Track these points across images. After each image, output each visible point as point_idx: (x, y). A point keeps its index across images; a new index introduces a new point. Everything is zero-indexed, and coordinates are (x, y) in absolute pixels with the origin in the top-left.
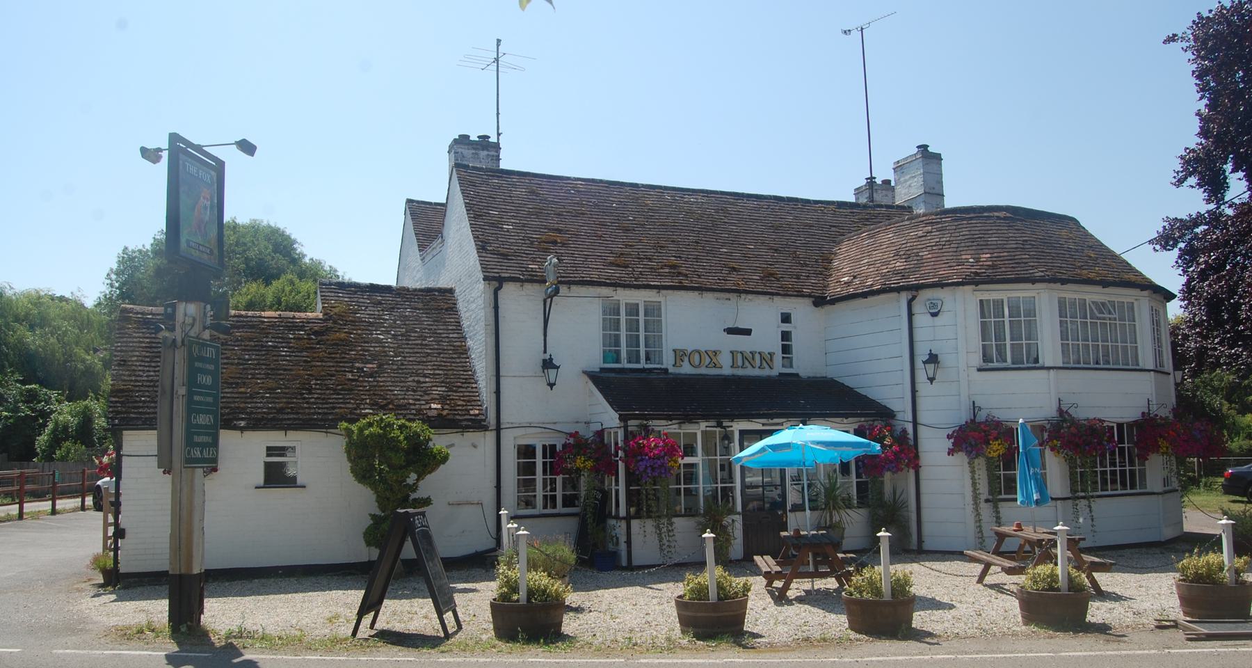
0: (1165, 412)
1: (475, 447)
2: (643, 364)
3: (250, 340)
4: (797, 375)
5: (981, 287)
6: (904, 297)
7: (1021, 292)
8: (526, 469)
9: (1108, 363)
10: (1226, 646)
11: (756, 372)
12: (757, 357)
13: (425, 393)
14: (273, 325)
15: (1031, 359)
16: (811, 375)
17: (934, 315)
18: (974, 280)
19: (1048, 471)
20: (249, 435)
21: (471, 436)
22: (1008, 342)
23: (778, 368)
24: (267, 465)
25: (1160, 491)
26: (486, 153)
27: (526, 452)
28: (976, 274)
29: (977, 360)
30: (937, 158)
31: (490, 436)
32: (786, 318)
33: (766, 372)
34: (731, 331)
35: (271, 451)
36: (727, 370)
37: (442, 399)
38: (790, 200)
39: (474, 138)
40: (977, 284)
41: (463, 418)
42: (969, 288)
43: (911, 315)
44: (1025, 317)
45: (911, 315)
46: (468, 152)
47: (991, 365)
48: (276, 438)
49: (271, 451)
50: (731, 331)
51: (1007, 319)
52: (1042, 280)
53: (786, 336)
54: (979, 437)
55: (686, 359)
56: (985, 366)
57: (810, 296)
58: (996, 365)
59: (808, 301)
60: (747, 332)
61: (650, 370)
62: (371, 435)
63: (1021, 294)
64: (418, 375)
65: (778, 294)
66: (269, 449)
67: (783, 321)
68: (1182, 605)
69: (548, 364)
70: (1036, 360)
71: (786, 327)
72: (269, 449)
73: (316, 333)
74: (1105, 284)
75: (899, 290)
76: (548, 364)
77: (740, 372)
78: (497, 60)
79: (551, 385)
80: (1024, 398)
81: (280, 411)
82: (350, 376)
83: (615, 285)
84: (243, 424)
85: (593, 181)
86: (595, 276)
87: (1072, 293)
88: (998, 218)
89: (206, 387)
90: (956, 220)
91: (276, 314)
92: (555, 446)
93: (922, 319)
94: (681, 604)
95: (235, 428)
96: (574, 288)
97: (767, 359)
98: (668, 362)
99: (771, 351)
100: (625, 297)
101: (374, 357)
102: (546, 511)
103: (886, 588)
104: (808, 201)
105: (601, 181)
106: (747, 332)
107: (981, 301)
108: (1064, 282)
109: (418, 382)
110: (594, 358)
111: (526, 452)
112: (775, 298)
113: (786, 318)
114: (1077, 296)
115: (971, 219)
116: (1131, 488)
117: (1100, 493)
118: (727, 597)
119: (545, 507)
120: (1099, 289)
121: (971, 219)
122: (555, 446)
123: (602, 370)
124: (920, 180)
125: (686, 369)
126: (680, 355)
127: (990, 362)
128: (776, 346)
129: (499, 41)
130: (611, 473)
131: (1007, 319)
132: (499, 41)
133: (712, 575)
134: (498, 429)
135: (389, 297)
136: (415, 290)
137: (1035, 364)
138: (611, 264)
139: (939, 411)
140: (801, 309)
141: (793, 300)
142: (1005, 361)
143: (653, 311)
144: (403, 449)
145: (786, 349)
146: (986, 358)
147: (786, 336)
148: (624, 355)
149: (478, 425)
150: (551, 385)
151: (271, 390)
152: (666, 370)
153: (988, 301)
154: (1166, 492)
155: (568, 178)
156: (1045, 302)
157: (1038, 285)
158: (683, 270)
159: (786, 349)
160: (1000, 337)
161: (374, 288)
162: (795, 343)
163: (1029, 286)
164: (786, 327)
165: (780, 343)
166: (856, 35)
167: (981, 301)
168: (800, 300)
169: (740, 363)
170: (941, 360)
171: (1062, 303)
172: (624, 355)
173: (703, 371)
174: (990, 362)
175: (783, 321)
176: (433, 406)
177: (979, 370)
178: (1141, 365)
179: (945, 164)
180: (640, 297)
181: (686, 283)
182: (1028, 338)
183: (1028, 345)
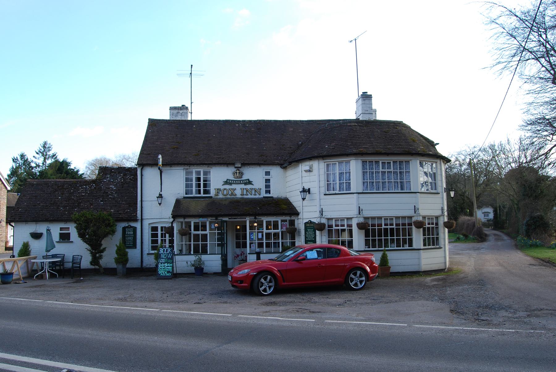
0: (75, 225)
4: (272, 197)
8: (154, 235)
10: (180, 309)
11: (253, 196)
19: (353, 238)
23: (263, 194)
24: (60, 234)
25: (363, 250)
29: (323, 190)
30: (370, 97)
32: (268, 173)
33: (257, 196)
35: (61, 229)
53: (268, 181)
56: (328, 193)
69: (160, 196)
71: (268, 177)
76: (160, 196)
78: (191, 74)
79: (160, 204)
97: (258, 191)
111: (154, 229)
113: (268, 173)
116: (434, 245)
123: (184, 198)
125: (221, 196)
129: (192, 66)
132: (192, 66)
136: (130, 168)
140: (276, 172)
145: (268, 186)
147: (268, 181)
159: (268, 186)
162: (272, 184)
164: (268, 177)
165: (264, 184)
169: (245, 193)
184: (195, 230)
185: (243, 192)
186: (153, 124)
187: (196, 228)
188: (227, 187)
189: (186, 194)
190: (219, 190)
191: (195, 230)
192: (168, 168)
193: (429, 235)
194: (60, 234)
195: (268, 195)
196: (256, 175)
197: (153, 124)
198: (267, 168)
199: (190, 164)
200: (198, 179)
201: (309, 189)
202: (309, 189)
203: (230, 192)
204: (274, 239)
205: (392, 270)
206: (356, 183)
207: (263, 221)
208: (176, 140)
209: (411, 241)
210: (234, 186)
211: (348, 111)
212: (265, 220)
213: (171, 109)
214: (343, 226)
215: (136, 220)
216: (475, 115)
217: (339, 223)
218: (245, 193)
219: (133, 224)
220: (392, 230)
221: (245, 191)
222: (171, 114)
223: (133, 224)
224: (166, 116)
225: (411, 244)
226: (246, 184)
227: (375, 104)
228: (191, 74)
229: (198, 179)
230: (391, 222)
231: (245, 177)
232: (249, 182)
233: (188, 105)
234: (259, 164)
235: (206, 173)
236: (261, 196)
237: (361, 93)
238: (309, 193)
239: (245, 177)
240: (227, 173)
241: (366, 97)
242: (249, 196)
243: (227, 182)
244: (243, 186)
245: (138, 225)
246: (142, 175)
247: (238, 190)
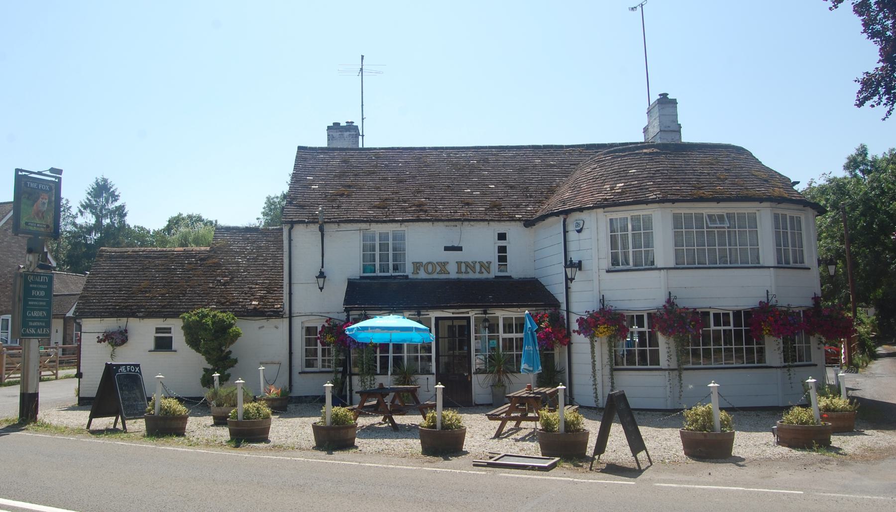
1: (277, 328)
2: (391, 273)
3: (163, 265)
4: (510, 277)
5: (606, 209)
6: (562, 218)
7: (641, 211)
9: (736, 262)
11: (477, 276)
12: (463, 266)
13: (252, 295)
14: (178, 256)
15: (649, 262)
16: (522, 277)
17: (579, 231)
18: (604, 205)
20: (147, 321)
21: (274, 321)
22: (631, 250)
26: (348, 133)
27: (309, 330)
28: (606, 200)
29: (606, 263)
31: (286, 322)
33: (485, 275)
34: (447, 249)
36: (453, 275)
37: (261, 299)
38: (545, 147)
39: (343, 124)
40: (604, 207)
41: (267, 312)
42: (600, 210)
43: (565, 232)
44: (644, 228)
45: (565, 232)
46: (336, 134)
47: (617, 268)
48: (160, 323)
49: (158, 330)
50: (447, 249)
51: (630, 233)
52: (653, 201)
53: (502, 249)
54: (607, 320)
55: (422, 269)
56: (613, 268)
57: (519, 220)
58: (621, 267)
59: (520, 224)
60: (460, 249)
61: (395, 277)
62: (193, 321)
63: (641, 213)
64: (253, 284)
65: (492, 220)
66: (157, 329)
67: (499, 239)
68: (684, 448)
69: (322, 275)
70: (653, 263)
71: (502, 243)
72: (157, 329)
73: (201, 260)
74: (718, 200)
75: (557, 214)
76: (322, 275)
77: (464, 276)
78: (362, 69)
79: (321, 289)
80: (640, 292)
81: (163, 307)
82: (211, 285)
83: (370, 221)
84: (141, 314)
85: (393, 149)
86: (357, 217)
87: (684, 209)
88: (645, 154)
89: (41, 297)
90: (613, 158)
91: (182, 249)
92: (316, 328)
93: (573, 235)
94: (316, 427)
95: (137, 317)
96: (342, 225)
97: (485, 266)
98: (409, 271)
99: (489, 260)
100: (377, 229)
101: (231, 273)
102: (324, 369)
103: (559, 427)
104: (561, 147)
105: (398, 148)
106: (460, 249)
107: (611, 220)
108: (673, 201)
109: (251, 288)
110: (355, 270)
111: (309, 330)
112: (491, 223)
113: (502, 237)
114: (693, 211)
115: (625, 156)
117: (798, 363)
118: (249, 418)
119: (323, 366)
120: (714, 204)
121: (625, 156)
122: (316, 328)
123: (362, 278)
124: (657, 121)
125: (422, 275)
126: (417, 266)
127: (617, 264)
128: (493, 257)
129: (363, 57)
130: (562, 343)
131: (630, 233)
132: (363, 57)
133: (330, 410)
134: (290, 317)
135: (255, 235)
137: (651, 266)
138: (375, 207)
139: (582, 302)
140: (515, 231)
141: (508, 223)
142: (628, 264)
143: (399, 238)
144: (211, 330)
145: (502, 259)
146: (615, 261)
147: (502, 249)
148: (377, 267)
149: (277, 314)
150: (321, 289)
151: (163, 295)
152: (407, 277)
153: (616, 219)
154: (784, 367)
155: (375, 149)
156: (661, 221)
157: (650, 206)
158: (426, 208)
159: (502, 259)
160: (625, 246)
161: (248, 230)
162: (509, 254)
163: (644, 206)
164: (502, 243)
165: (497, 254)
166: (639, 9)
167: (611, 220)
168: (513, 223)
169: (463, 269)
170: (593, 265)
171: (677, 219)
172: (377, 267)
173: (435, 276)
174: (617, 264)
175: (499, 239)
176: (254, 303)
177: (608, 271)
178: (762, 263)
179: (679, 106)
180: (389, 229)
181: (423, 217)
182: (647, 246)
183: (647, 252)
184: (505, 332)
185: (459, 267)
186: (303, 152)
187: (508, 328)
191: (505, 332)
194: (708, 313)
197: (303, 152)
198: (502, 227)
201: (580, 262)
202: (580, 262)
203: (438, 269)
204: (725, 344)
206: (663, 250)
207: (498, 317)
208: (341, 179)
209: (761, 351)
211: (629, 127)
212: (501, 314)
216: (812, 138)
218: (463, 269)
221: (463, 266)
222: (330, 138)
224: (322, 141)
225: (761, 359)
227: (683, 117)
228: (362, 69)
233: (357, 123)
236: (491, 276)
237: (655, 97)
238: (580, 269)
241: (666, 103)
246: (290, 240)
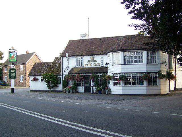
11: (97, 66)
23: (101, 65)
32: (102, 58)
33: (99, 66)
53: (102, 60)
71: (102, 59)
113: (102, 58)
125: (87, 66)
140: (105, 57)
147: (102, 60)
165: (101, 61)
188: (89, 63)
189: (102, 65)
190: (86, 64)
192: (70, 57)
193: (116, 81)
194: (41, 79)
195: (102, 66)
196: (98, 58)
199: (77, 56)
200: (79, 61)
205: (112, 93)
206: (145, 61)
208: (76, 48)
210: (91, 63)
213: (81, 35)
214: (135, 76)
215: (61, 75)
217: (134, 75)
219: (60, 76)
220: (154, 78)
223: (60, 76)
226: (95, 62)
229: (79, 61)
230: (154, 75)
231: (94, 59)
232: (96, 61)
234: (99, 55)
235: (82, 58)
239: (94, 59)
240: (89, 58)
242: (96, 66)
243: (89, 61)
244: (94, 63)
245: (61, 76)
247: (92, 65)
